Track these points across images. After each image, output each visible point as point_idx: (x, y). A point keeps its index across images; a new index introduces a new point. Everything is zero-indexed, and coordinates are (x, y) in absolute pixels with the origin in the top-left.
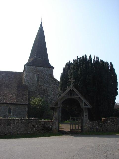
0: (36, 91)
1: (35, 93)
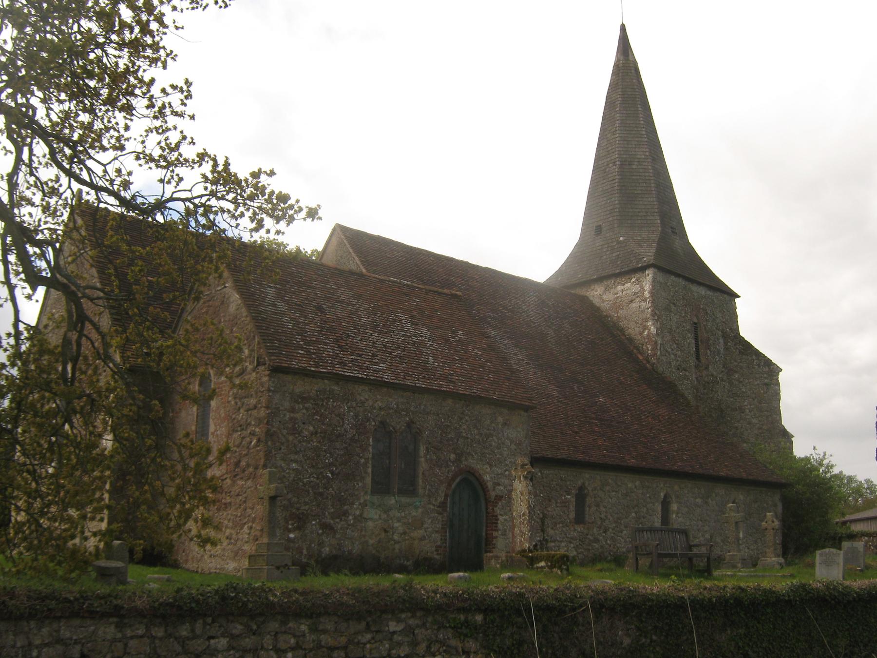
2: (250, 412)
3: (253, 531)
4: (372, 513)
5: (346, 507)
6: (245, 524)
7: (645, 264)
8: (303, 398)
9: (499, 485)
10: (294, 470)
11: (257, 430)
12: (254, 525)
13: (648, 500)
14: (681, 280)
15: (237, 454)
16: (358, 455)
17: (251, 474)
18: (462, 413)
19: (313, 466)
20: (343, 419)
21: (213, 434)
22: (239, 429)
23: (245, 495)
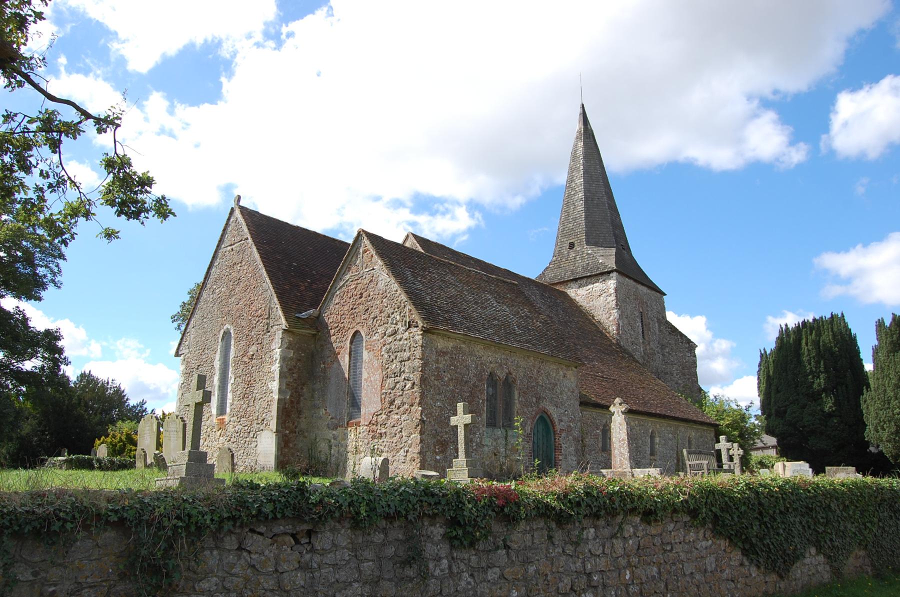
2: (403, 363)
3: (409, 454)
4: (487, 441)
6: (401, 448)
7: (609, 270)
9: (562, 421)
10: (439, 407)
11: (411, 376)
12: (410, 449)
13: (643, 434)
14: (632, 281)
15: (392, 395)
16: (478, 397)
17: (407, 410)
18: (539, 368)
20: (468, 369)
21: (365, 379)
22: (393, 376)
23: (400, 426)
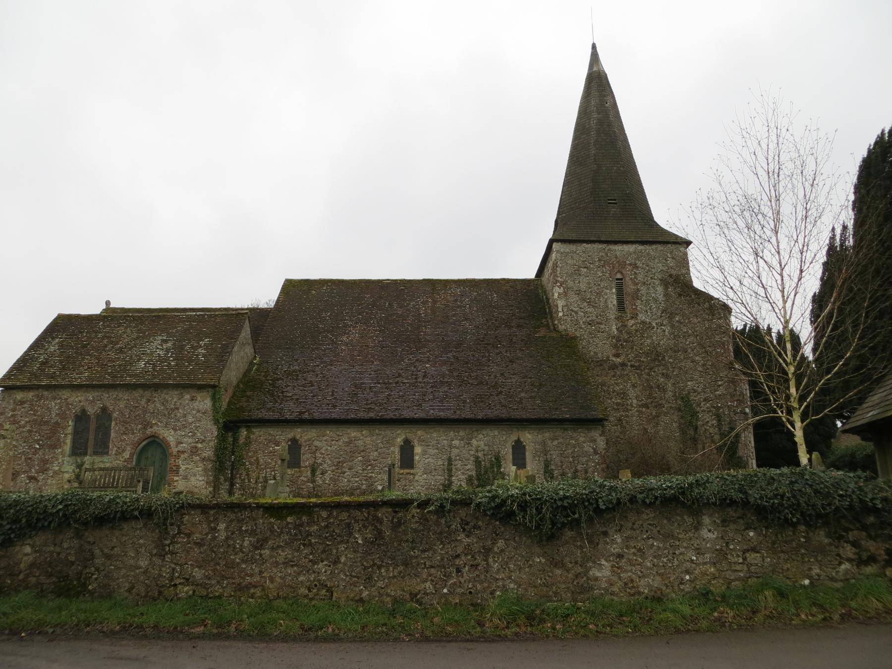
0: (617, 355)
1: (614, 367)
5: (48, 466)
8: (22, 402)
19: (25, 442)
